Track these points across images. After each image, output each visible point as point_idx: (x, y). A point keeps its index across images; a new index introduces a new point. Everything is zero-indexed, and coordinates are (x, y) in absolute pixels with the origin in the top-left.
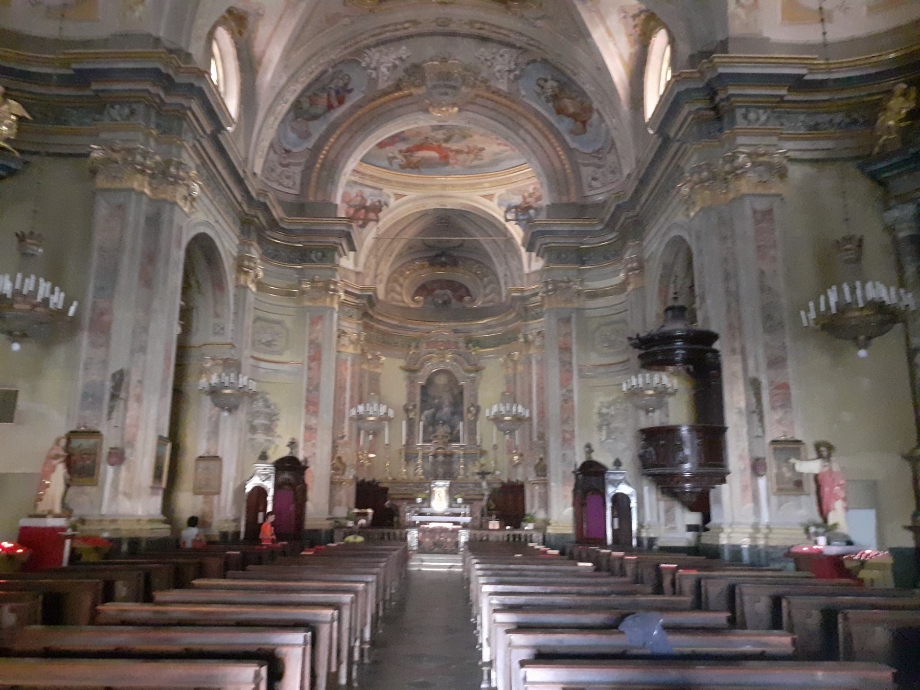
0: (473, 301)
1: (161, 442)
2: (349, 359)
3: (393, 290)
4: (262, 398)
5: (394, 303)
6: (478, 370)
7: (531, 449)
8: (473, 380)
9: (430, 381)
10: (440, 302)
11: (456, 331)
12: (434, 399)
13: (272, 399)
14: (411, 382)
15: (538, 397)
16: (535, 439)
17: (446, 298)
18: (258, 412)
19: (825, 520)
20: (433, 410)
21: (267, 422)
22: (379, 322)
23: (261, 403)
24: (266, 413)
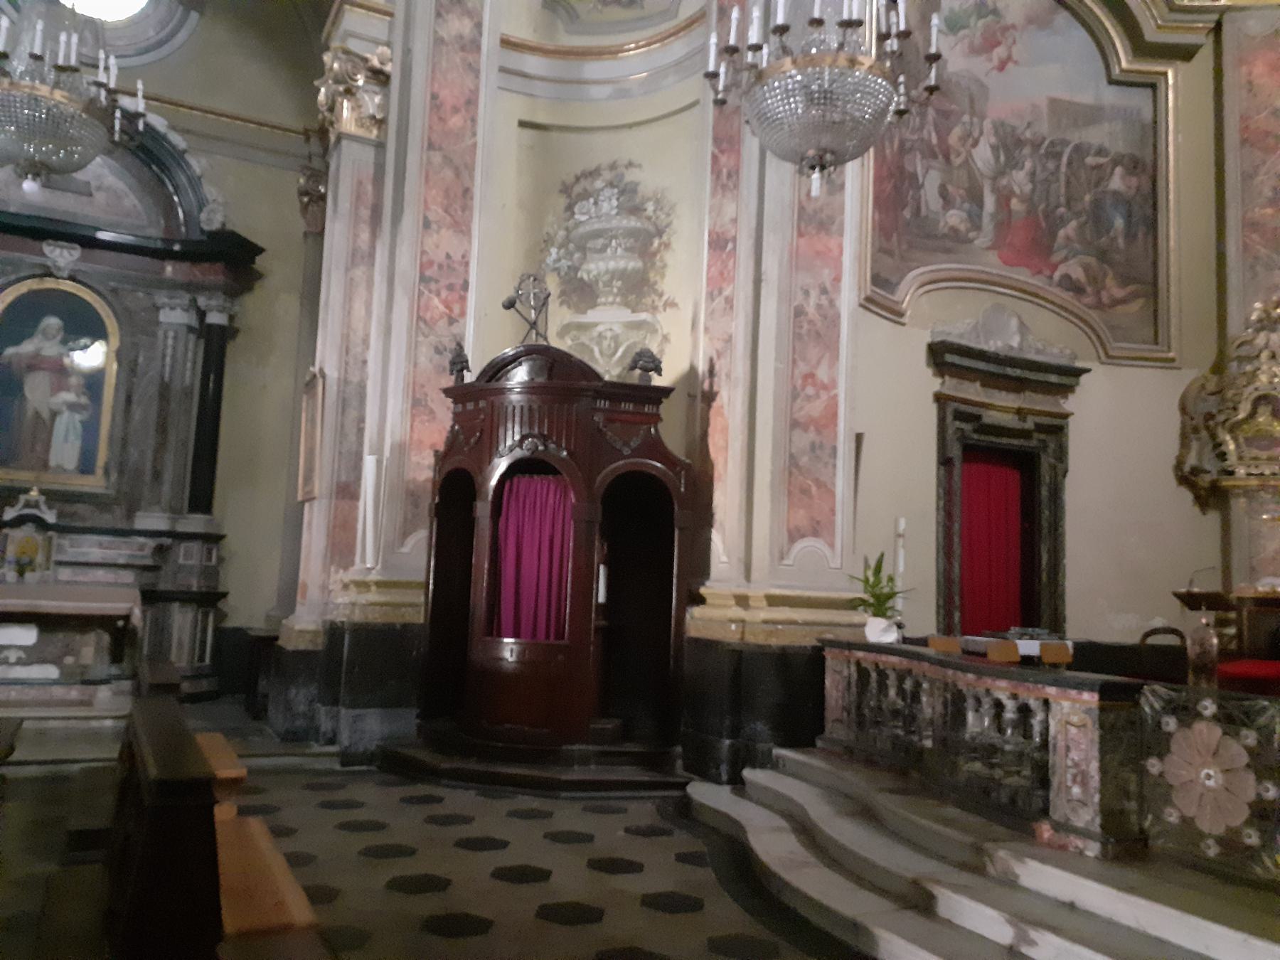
1: (495, 633)
4: (611, 185)
13: (647, 179)
18: (597, 234)
19: (896, 188)
21: (634, 264)
23: (609, 204)
24: (632, 233)
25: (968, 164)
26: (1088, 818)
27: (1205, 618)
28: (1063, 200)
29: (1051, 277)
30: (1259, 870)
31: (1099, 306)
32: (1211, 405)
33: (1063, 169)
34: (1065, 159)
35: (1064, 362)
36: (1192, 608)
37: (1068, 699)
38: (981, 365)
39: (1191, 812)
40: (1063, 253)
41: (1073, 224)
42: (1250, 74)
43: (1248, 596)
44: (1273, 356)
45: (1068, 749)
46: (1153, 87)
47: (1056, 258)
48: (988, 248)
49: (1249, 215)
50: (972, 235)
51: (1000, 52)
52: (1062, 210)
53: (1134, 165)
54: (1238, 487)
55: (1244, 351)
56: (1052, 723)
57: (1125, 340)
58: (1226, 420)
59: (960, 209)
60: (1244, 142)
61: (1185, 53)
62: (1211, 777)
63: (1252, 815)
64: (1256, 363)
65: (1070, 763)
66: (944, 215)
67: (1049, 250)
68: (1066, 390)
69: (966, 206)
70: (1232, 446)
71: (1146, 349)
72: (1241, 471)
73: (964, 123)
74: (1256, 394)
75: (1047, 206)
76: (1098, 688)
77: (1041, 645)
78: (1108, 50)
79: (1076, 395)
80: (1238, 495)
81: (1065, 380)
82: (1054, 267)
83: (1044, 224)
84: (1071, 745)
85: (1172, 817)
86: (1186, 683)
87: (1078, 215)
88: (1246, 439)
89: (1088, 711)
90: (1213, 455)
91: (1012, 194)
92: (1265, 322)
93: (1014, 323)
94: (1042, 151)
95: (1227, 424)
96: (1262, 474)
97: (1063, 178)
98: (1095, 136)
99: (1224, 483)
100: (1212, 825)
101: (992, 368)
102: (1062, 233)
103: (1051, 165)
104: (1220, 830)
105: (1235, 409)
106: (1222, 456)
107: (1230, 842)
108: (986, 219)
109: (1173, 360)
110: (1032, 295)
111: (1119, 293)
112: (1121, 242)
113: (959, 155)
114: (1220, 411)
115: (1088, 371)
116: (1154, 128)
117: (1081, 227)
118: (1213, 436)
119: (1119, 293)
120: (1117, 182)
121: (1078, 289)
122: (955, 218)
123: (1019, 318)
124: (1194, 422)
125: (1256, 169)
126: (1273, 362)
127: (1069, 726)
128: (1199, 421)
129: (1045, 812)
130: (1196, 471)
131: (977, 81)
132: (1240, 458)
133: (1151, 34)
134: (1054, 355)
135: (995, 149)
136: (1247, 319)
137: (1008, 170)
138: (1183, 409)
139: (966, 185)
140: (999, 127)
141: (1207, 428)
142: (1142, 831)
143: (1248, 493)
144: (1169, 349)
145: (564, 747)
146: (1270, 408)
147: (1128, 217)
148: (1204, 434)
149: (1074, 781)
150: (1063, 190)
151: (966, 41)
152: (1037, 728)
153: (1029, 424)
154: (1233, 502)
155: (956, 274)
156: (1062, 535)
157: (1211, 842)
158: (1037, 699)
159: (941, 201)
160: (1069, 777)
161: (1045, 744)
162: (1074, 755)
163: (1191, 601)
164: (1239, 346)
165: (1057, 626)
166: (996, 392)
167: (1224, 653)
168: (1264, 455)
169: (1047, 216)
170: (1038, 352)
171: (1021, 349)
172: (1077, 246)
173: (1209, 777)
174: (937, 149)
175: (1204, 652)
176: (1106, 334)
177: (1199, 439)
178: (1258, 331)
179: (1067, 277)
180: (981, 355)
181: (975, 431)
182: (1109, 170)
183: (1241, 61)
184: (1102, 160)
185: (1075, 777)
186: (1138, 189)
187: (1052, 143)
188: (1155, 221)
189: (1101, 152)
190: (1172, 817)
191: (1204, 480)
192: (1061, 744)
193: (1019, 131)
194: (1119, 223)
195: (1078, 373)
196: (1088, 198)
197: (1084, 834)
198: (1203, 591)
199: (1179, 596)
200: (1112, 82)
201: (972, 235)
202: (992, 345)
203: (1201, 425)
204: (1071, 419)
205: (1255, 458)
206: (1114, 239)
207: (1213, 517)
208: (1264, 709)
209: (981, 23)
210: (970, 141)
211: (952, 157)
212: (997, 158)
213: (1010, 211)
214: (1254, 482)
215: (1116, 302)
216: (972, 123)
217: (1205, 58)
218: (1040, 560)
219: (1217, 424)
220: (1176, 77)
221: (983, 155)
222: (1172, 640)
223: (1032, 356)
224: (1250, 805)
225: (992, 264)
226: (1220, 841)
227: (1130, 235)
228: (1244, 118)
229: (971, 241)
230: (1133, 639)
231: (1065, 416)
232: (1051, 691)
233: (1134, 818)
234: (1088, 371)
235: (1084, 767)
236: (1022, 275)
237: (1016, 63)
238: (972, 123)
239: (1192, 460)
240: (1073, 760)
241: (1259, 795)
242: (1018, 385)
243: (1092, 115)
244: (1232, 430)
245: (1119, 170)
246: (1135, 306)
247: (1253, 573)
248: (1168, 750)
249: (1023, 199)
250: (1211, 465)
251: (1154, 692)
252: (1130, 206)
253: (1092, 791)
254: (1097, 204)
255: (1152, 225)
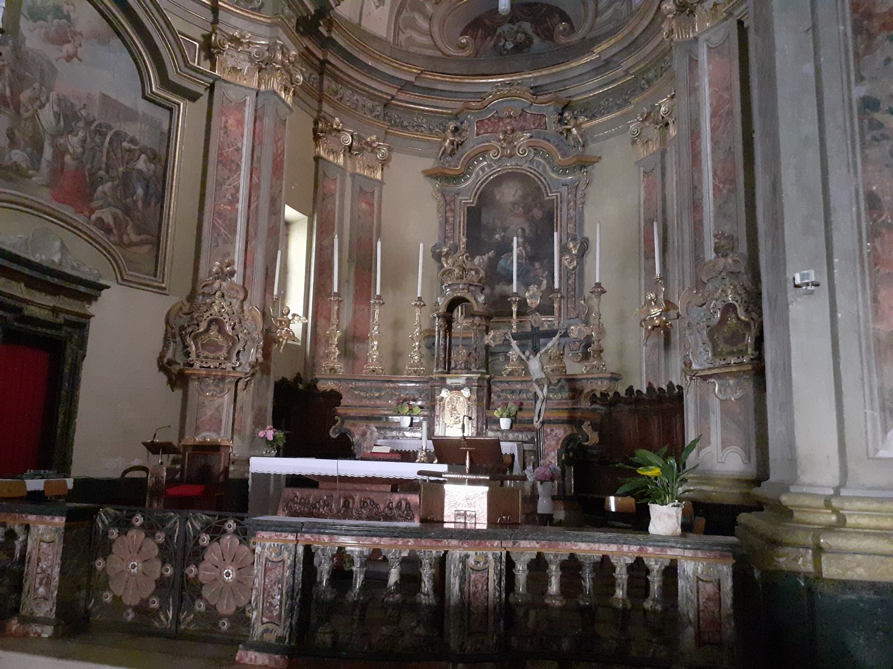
0: (572, 29)
2: (250, 100)
3: (413, 25)
5: (412, 49)
6: (583, 164)
7: (699, 284)
8: (574, 188)
9: (485, 198)
10: (510, 46)
11: (536, 90)
12: (493, 231)
14: (447, 202)
15: (698, 105)
16: (710, 254)
17: (520, 37)
20: (491, 254)
22: (371, 71)
25: (34, 118)
26: (48, 609)
27: (159, 459)
28: (103, 166)
29: (90, 218)
30: (156, 624)
31: (121, 244)
32: (184, 320)
33: (106, 144)
34: (108, 138)
35: (90, 278)
36: (154, 453)
37: (44, 523)
38: (27, 271)
39: (119, 592)
40: (101, 202)
41: (109, 184)
42: (227, 122)
43: (189, 444)
44: (223, 296)
45: (39, 560)
46: (171, 110)
47: (94, 204)
48: (43, 185)
49: (218, 207)
50: (31, 172)
51: (68, 48)
52: (102, 173)
53: (153, 157)
54: (195, 374)
55: (206, 290)
56: (29, 541)
57: (134, 270)
58: (192, 332)
59: (24, 150)
60: (219, 162)
61: (193, 97)
62: (135, 566)
63: (157, 588)
64: (213, 299)
65: (39, 570)
66: (9, 152)
67: (91, 199)
68: (90, 299)
69: (29, 150)
70: (194, 348)
71: (148, 279)
72: (197, 365)
73: (34, 89)
74: (211, 317)
75: (93, 167)
76: (65, 513)
77: (45, 483)
78: (144, 72)
79: (98, 303)
80: (194, 380)
81: (92, 292)
82: (92, 211)
83: (88, 179)
84: (41, 557)
85: (108, 598)
86: (144, 505)
87: (113, 179)
88: (202, 345)
89: (57, 530)
90: (181, 353)
91: (66, 151)
92: (220, 274)
93: (57, 244)
94: (93, 128)
95: (193, 334)
96: (209, 367)
97: (105, 151)
98: (131, 129)
99: (186, 372)
100: (131, 599)
101: (36, 275)
102: (100, 188)
103: (97, 139)
104: (135, 602)
105: (198, 325)
106: (188, 354)
107: (142, 609)
108: (44, 164)
109: (164, 289)
110: (74, 228)
111: (134, 237)
112: (140, 204)
113: (27, 110)
114: (189, 326)
115: (108, 287)
116: (169, 136)
117: (114, 189)
118: (183, 341)
119: (134, 237)
120: (141, 164)
121: (108, 231)
122: (18, 156)
123: (62, 243)
124: (173, 331)
125: (224, 180)
126: (222, 300)
127: (41, 543)
128: (176, 330)
129: (16, 611)
130: (171, 362)
131: (49, 62)
132: (198, 356)
133: (172, 76)
134: (86, 272)
135: (57, 115)
136: (210, 270)
137: (65, 133)
138: (167, 322)
139: (31, 134)
140: (60, 100)
141: (181, 335)
142: (87, 611)
143: (200, 379)
144: (163, 282)
145: (613, 509)
146: (217, 327)
147: (147, 188)
148: (178, 339)
149: (41, 584)
150: (104, 159)
151: (43, 31)
152: (18, 547)
153: (60, 319)
154: (190, 384)
155: (13, 198)
156: (77, 402)
157: (130, 611)
158: (21, 525)
159: (8, 141)
160: (38, 580)
161: (23, 556)
162: (44, 565)
163: (153, 448)
164: (205, 286)
165: (64, 468)
166: (37, 294)
167: (171, 482)
168: (211, 355)
169: (92, 175)
170: (73, 268)
171: (60, 264)
172: (110, 200)
173: (134, 567)
174: (9, 100)
175: (158, 482)
176: (122, 262)
177: (175, 342)
178: (216, 279)
179: (100, 219)
180: (28, 263)
181: (16, 320)
182: (137, 155)
183: (222, 113)
184: (133, 147)
185: (42, 580)
186: (155, 172)
187: (100, 125)
188: (163, 197)
189: (133, 141)
190: (108, 598)
191: (175, 369)
192: (34, 557)
193: (77, 108)
194: (140, 191)
195: (102, 287)
196: (121, 169)
197: (43, 621)
198: (162, 441)
199: (145, 444)
200: (145, 97)
201: (31, 172)
202: (37, 258)
203: (177, 333)
204: (92, 319)
205: (207, 357)
206: (135, 202)
207: (179, 392)
208: (171, 518)
209: (56, 21)
210: (38, 103)
211: (22, 110)
212: (58, 122)
213: (64, 163)
214: (203, 372)
215: (132, 244)
216: (40, 91)
217: (204, 100)
218: (57, 418)
219: (186, 334)
220: (185, 109)
221: (47, 117)
222: (142, 474)
223: (68, 271)
224: (156, 581)
225: (44, 197)
226: (136, 609)
227: (146, 202)
228: (221, 148)
229: (30, 177)
230: (117, 475)
231: (89, 317)
232: (32, 518)
233: (82, 603)
234: (108, 287)
235: (49, 572)
236: (67, 211)
237: (80, 60)
238: (40, 91)
239: (169, 355)
240: (42, 568)
241: (162, 574)
242: (54, 290)
243: (131, 115)
244: (195, 339)
245: (143, 156)
246: (146, 248)
247: (197, 430)
248: (111, 552)
249: (76, 158)
250: (180, 359)
251: (106, 513)
252: (148, 183)
253: (53, 588)
254: (127, 175)
255: (161, 199)
